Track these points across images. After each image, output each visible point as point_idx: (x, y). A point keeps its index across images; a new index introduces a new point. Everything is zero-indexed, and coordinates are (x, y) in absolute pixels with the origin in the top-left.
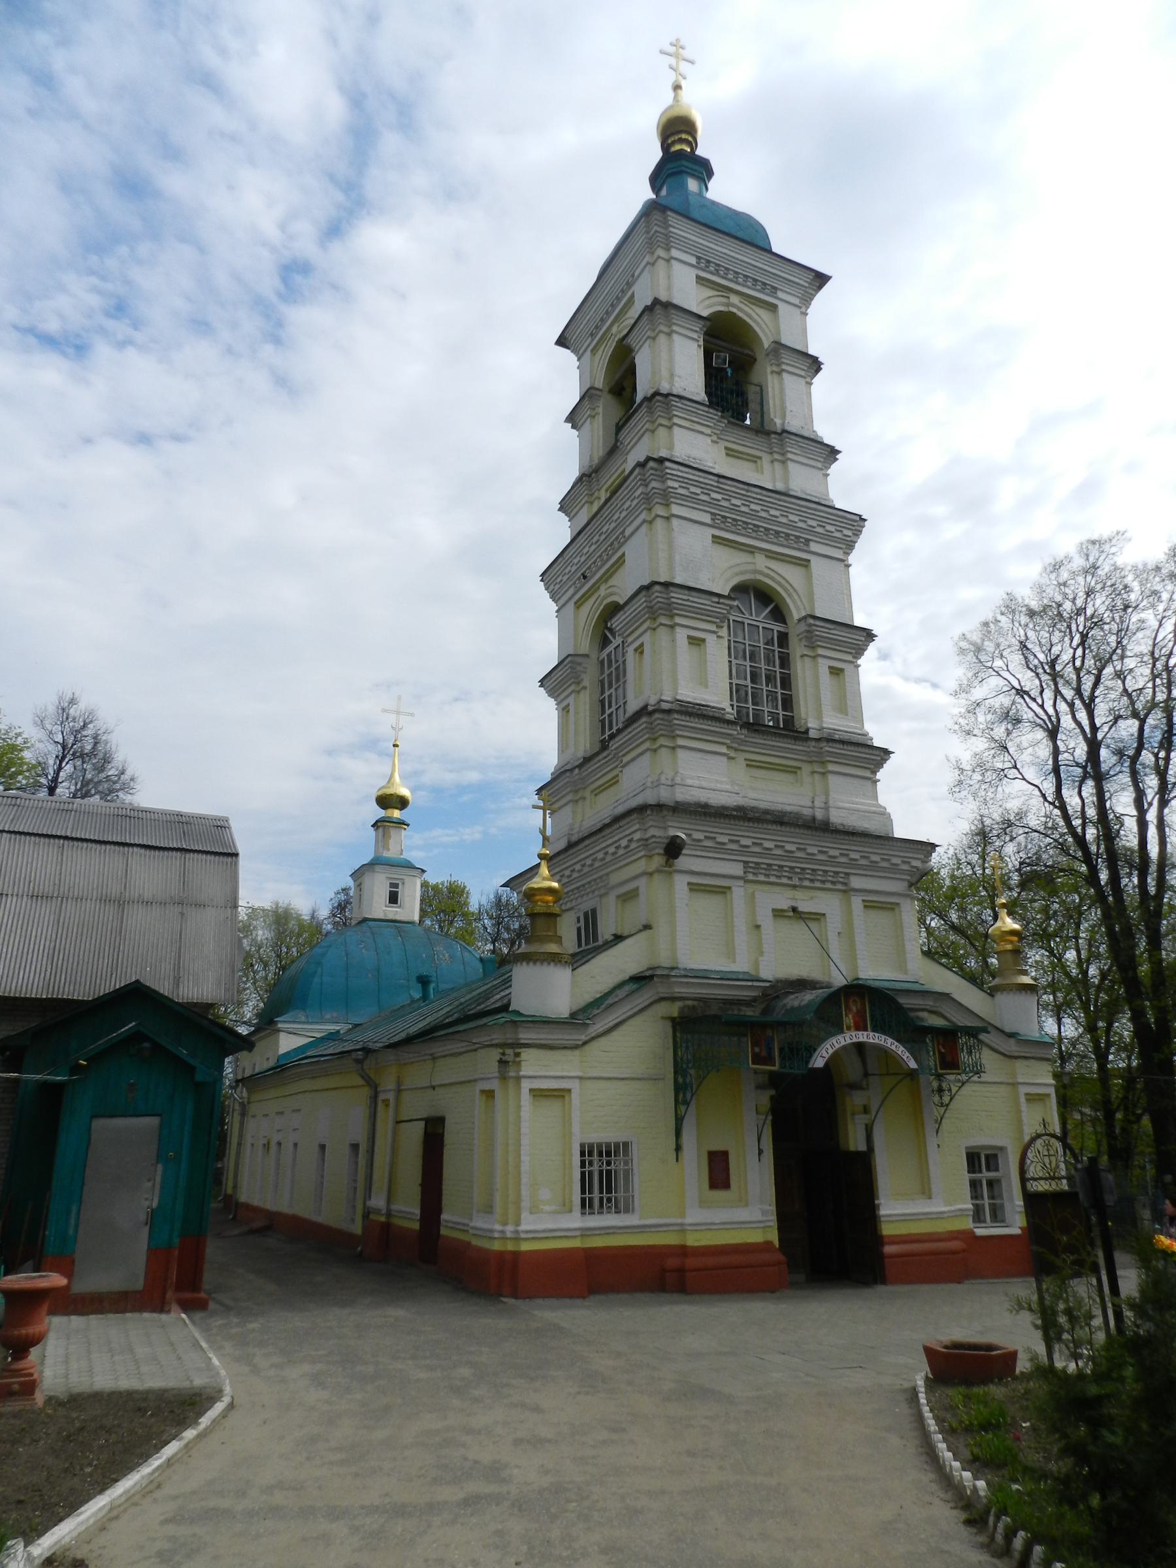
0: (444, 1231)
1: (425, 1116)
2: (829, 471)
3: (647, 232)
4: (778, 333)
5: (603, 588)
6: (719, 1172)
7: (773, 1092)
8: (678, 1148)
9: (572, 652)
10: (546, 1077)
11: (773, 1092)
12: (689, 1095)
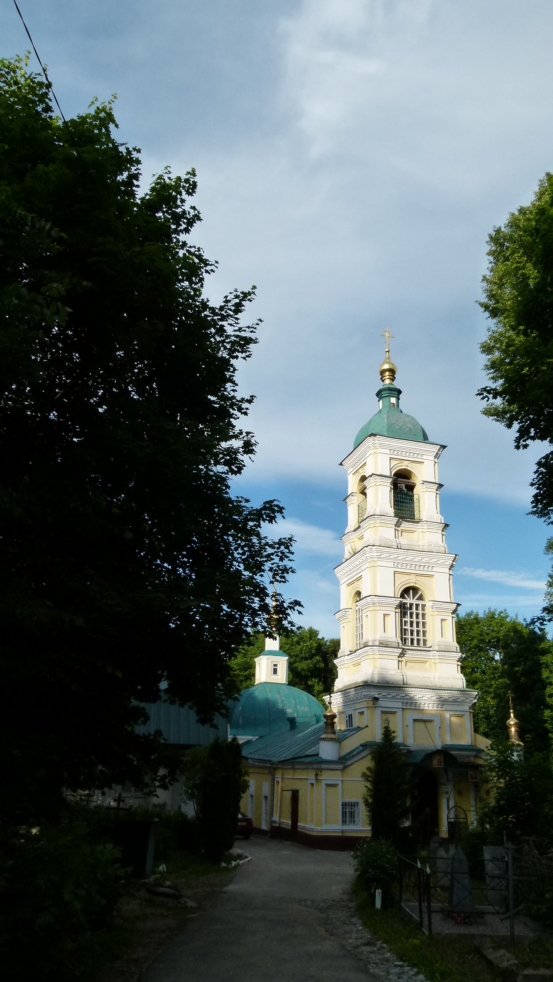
0: (299, 829)
7: (113, 785)
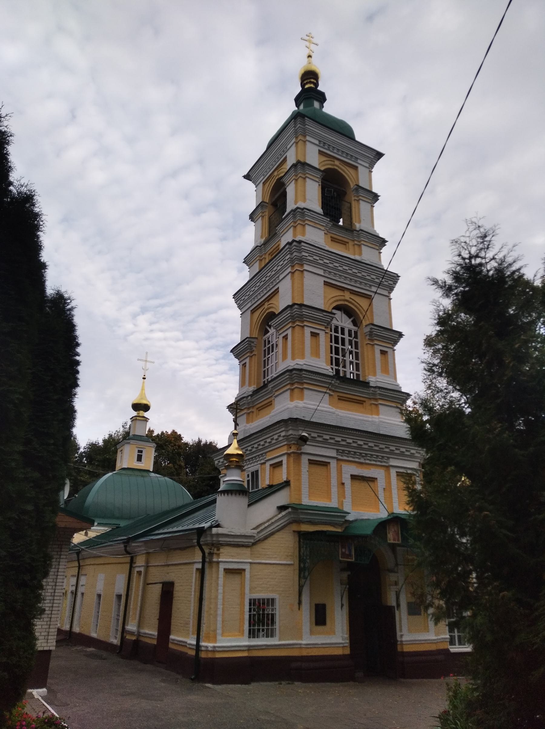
0: (171, 646)
1: (162, 581)
2: (381, 251)
3: (295, 127)
4: (358, 180)
5: (266, 304)
6: (320, 617)
7: (349, 573)
8: (300, 603)
9: (249, 336)
10: (232, 562)
11: (349, 573)
12: (307, 574)
